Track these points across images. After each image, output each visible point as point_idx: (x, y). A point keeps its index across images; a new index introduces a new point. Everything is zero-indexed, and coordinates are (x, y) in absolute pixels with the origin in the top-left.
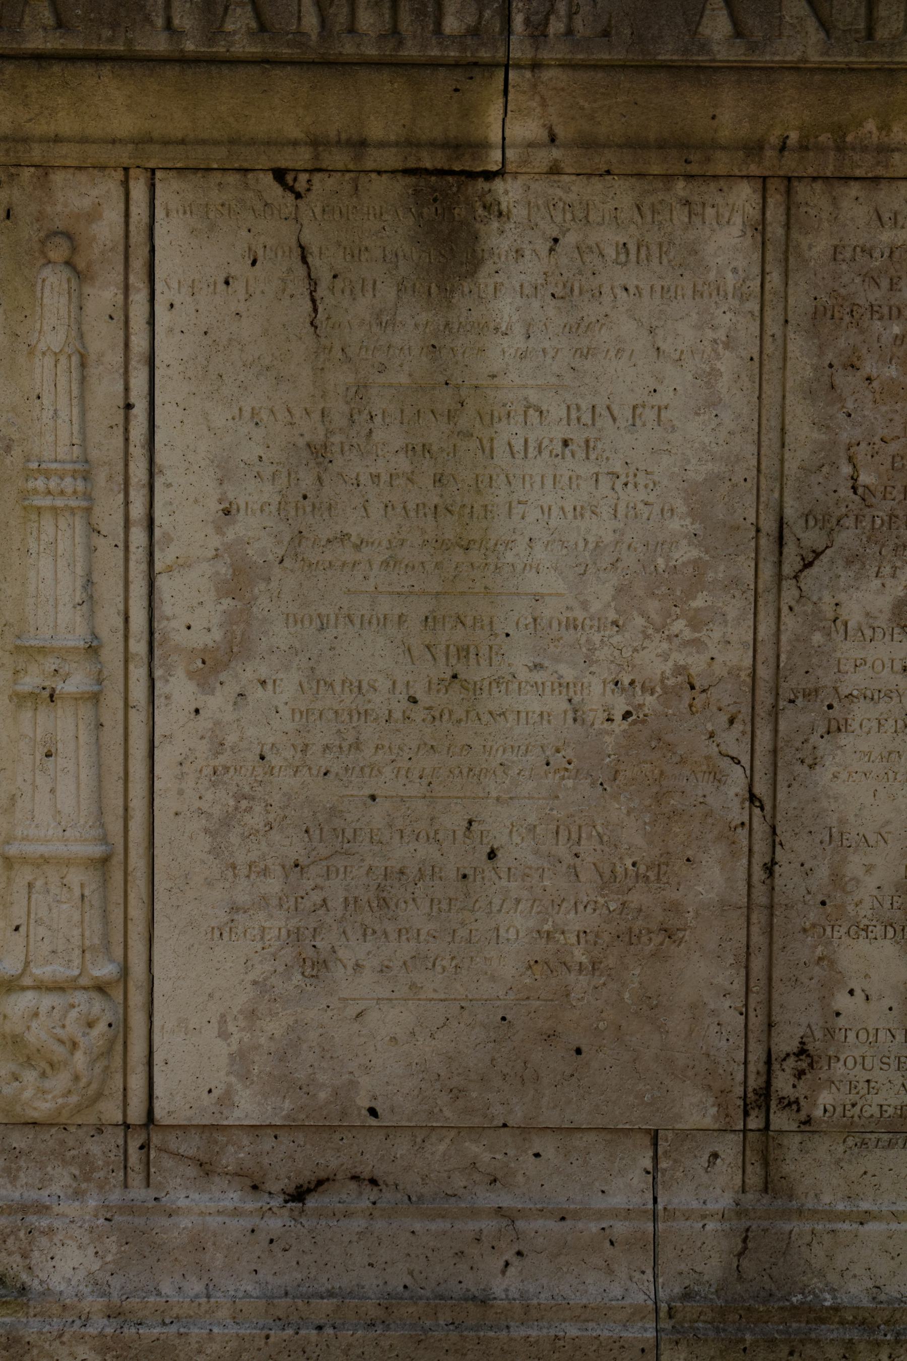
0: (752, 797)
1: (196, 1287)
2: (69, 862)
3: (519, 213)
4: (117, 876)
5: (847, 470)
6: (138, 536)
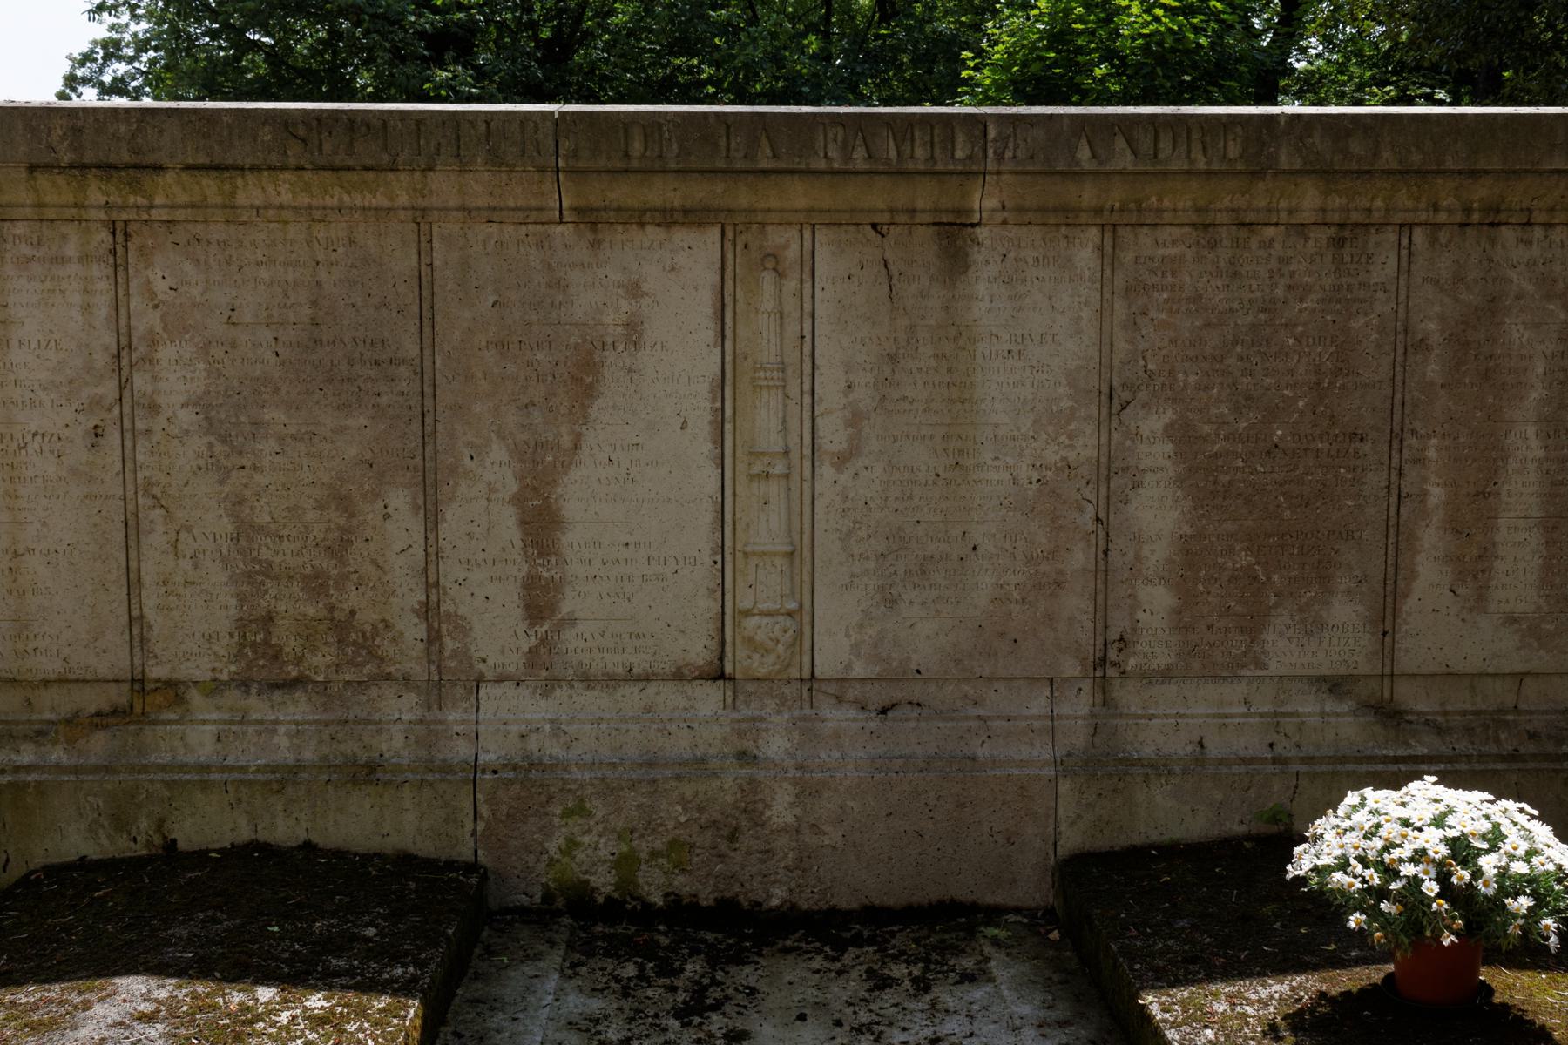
0: (1098, 519)
1: (836, 754)
2: (775, 554)
3: (988, 243)
4: (797, 561)
5: (1142, 363)
6: (807, 399)
